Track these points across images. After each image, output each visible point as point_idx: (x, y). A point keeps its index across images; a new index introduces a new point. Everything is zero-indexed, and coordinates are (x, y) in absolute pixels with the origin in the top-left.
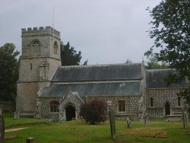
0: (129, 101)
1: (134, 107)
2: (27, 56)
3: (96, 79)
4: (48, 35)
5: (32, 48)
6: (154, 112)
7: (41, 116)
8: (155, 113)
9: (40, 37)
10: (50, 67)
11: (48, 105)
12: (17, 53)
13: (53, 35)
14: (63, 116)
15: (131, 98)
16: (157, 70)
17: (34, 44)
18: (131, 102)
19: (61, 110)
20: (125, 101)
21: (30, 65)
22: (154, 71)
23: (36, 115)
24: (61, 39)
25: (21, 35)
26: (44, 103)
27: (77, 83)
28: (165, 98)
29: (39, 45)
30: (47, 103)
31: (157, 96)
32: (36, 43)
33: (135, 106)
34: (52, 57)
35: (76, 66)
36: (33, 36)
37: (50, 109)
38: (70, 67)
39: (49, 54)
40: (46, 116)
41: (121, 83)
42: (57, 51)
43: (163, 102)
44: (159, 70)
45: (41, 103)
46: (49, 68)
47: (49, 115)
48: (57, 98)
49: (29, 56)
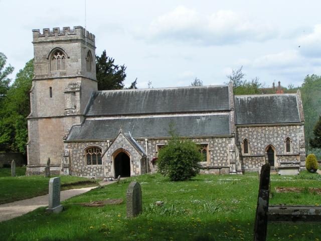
0: (213, 144)
1: (221, 155)
2: (42, 76)
3: (159, 112)
6: (250, 162)
8: (251, 163)
9: (65, 45)
12: (10, 70)
14: (109, 170)
15: (217, 141)
16: (253, 96)
17: (55, 56)
18: (217, 146)
21: (48, 91)
22: (248, 98)
23: (65, 170)
24: (96, 46)
26: (76, 151)
27: (127, 118)
28: (267, 140)
29: (63, 57)
30: (82, 151)
31: (255, 137)
33: (223, 152)
36: (52, 42)
37: (85, 159)
38: (113, 92)
41: (199, 118)
42: (91, 66)
43: (263, 146)
44: (256, 96)
47: (85, 169)
49: (47, 75)
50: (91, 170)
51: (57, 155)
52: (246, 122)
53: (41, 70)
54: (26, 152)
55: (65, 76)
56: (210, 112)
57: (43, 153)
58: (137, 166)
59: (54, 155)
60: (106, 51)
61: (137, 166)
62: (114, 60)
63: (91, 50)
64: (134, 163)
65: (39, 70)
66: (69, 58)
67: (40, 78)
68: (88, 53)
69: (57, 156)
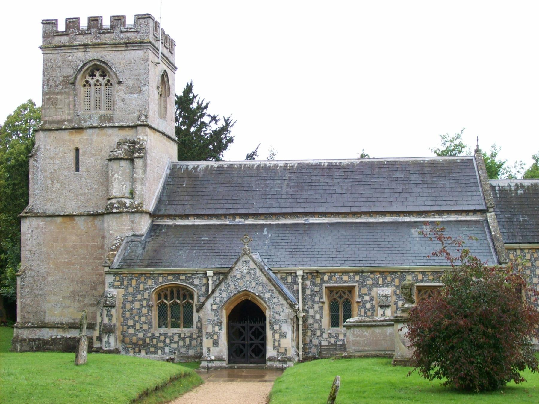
2: (59, 122)
4: (141, 44)
5: (82, 91)
7: (123, 341)
10: (149, 162)
11: (149, 300)
13: (159, 45)
14: (216, 343)
17: (89, 79)
19: (209, 321)
20: (351, 289)
21: (72, 156)
23: (105, 339)
25: (40, 43)
26: (134, 295)
29: (109, 81)
30: (146, 295)
32: (97, 73)
34: (156, 127)
35: (212, 163)
36: (85, 46)
38: (190, 167)
39: (146, 116)
40: (141, 342)
45: (120, 296)
46: (145, 165)
47: (153, 337)
48: (183, 274)
49: (70, 121)
50: (168, 341)
51: (86, 302)
52: (519, 238)
53: (56, 109)
54: (16, 293)
55: (111, 124)
56: (440, 213)
57: (53, 298)
58: (283, 336)
59: (79, 302)
60: (193, 83)
61: (283, 336)
62: (208, 104)
63: (169, 71)
64: (276, 327)
65: (54, 109)
66: (120, 83)
67: (55, 126)
68: (163, 75)
69: (85, 305)
